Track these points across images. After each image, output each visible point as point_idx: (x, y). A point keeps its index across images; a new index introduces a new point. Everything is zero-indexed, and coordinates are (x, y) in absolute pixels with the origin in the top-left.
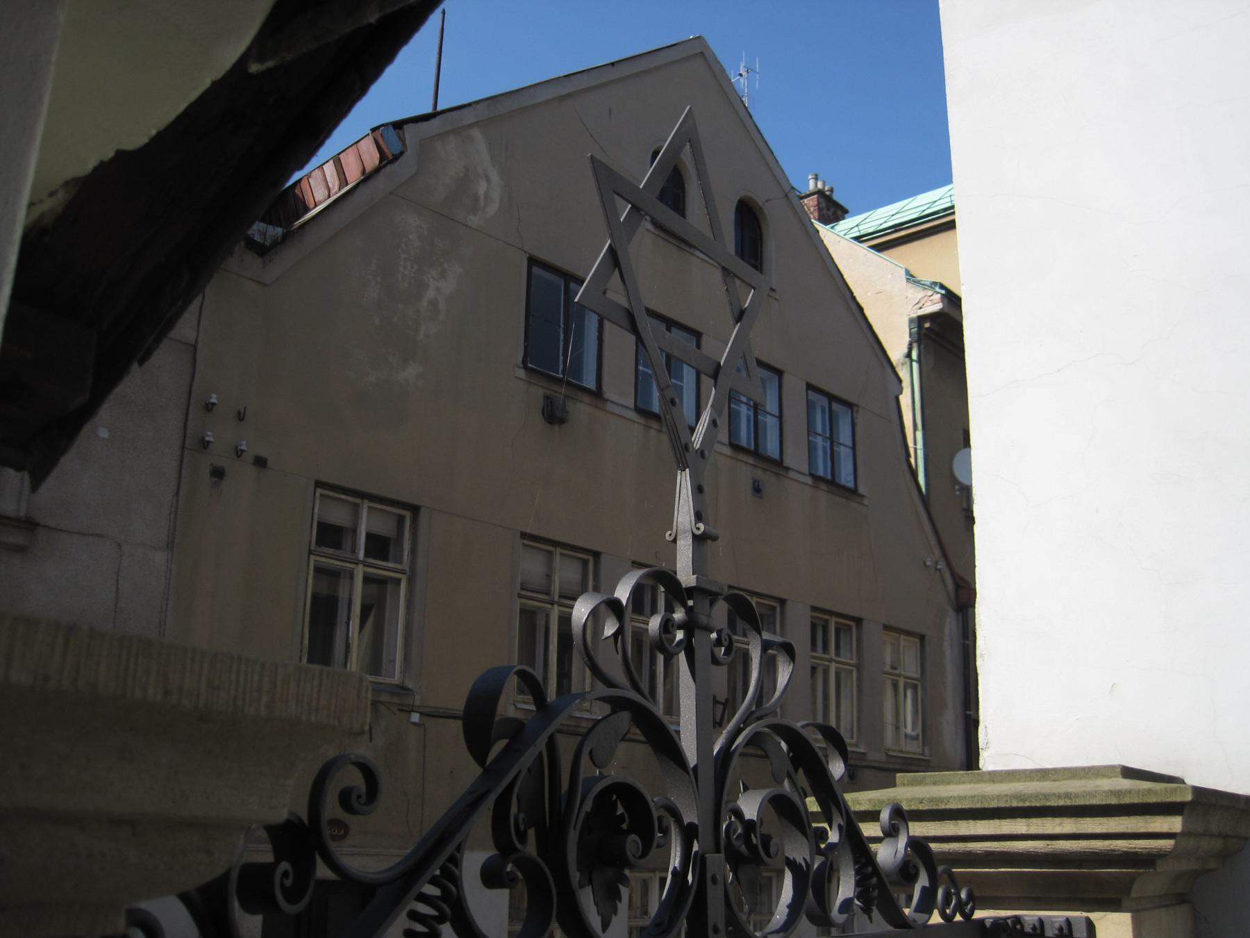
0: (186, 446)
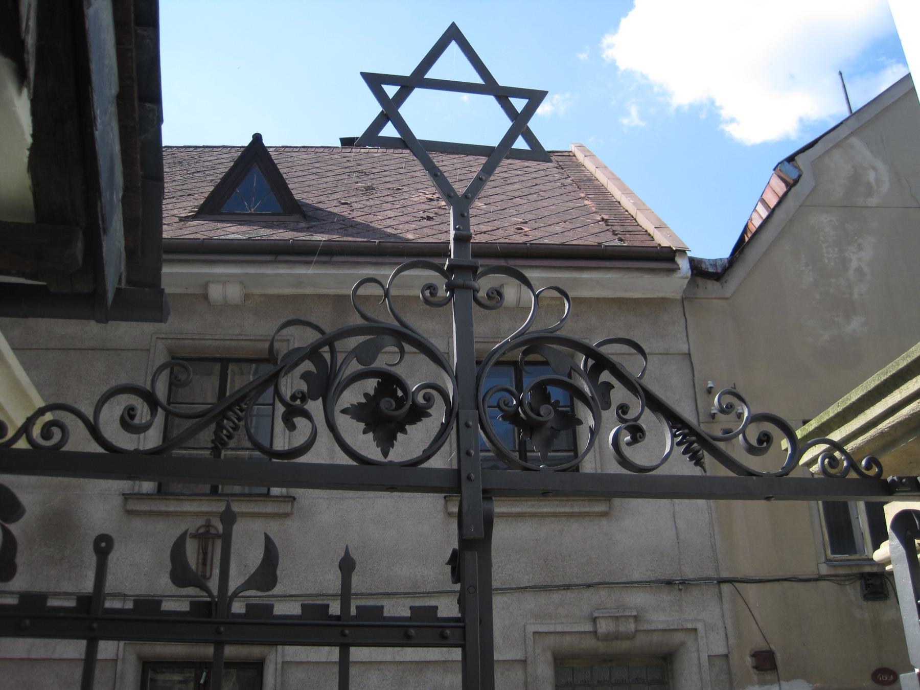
0: (701, 421)
